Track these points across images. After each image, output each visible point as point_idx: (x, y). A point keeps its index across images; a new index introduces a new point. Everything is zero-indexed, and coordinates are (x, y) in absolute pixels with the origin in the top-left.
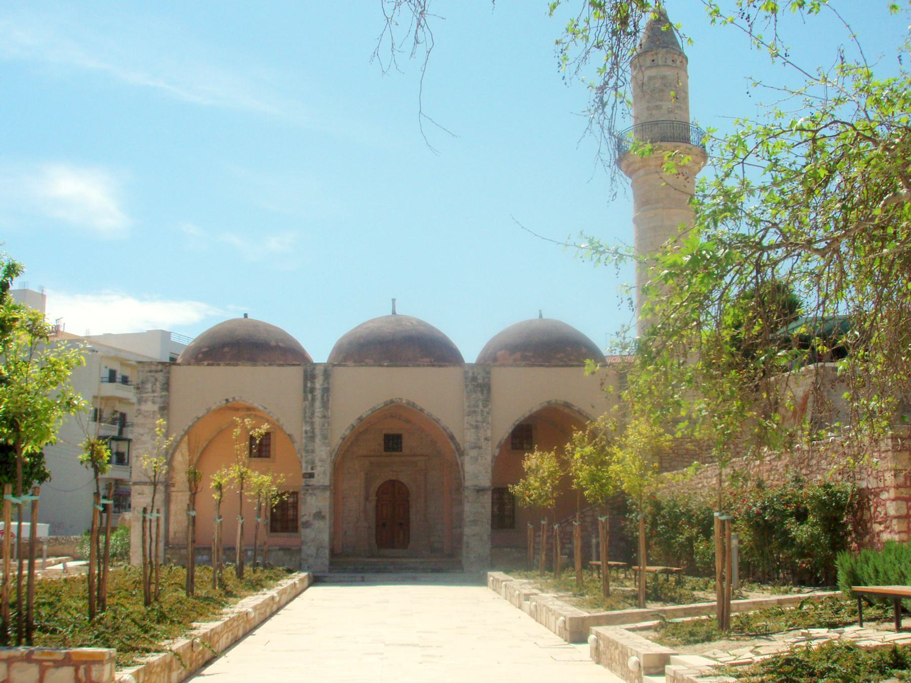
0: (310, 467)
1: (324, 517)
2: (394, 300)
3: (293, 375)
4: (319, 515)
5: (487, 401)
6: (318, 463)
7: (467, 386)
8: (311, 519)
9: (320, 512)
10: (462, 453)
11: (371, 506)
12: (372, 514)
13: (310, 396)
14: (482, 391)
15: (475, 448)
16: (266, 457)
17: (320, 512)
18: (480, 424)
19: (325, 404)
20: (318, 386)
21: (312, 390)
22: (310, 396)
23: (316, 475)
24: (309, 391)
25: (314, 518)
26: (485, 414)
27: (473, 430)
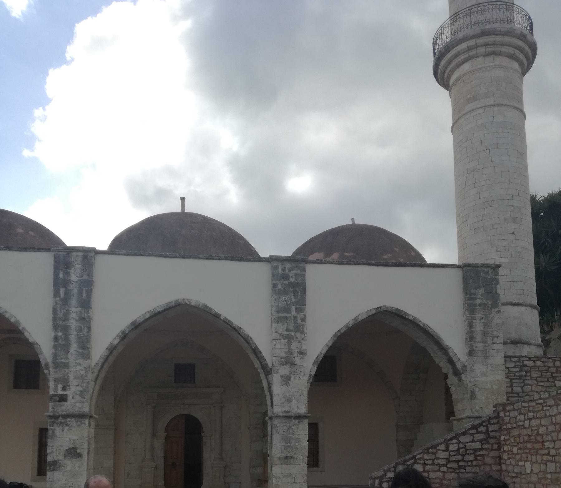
0: (60, 386)
1: (79, 455)
2: (183, 199)
3: (41, 263)
4: (73, 453)
5: (301, 304)
6: (73, 382)
7: (275, 286)
8: (60, 458)
9: (75, 449)
10: (268, 372)
11: (159, 444)
12: (160, 452)
13: (62, 291)
14: (295, 293)
15: (286, 363)
16: (34, 388)
17: (75, 449)
18: (293, 334)
19: (86, 304)
20: (74, 278)
21: (66, 283)
22: (62, 291)
23: (69, 398)
24: (60, 283)
25: (65, 456)
26: (299, 321)
27: (284, 342)
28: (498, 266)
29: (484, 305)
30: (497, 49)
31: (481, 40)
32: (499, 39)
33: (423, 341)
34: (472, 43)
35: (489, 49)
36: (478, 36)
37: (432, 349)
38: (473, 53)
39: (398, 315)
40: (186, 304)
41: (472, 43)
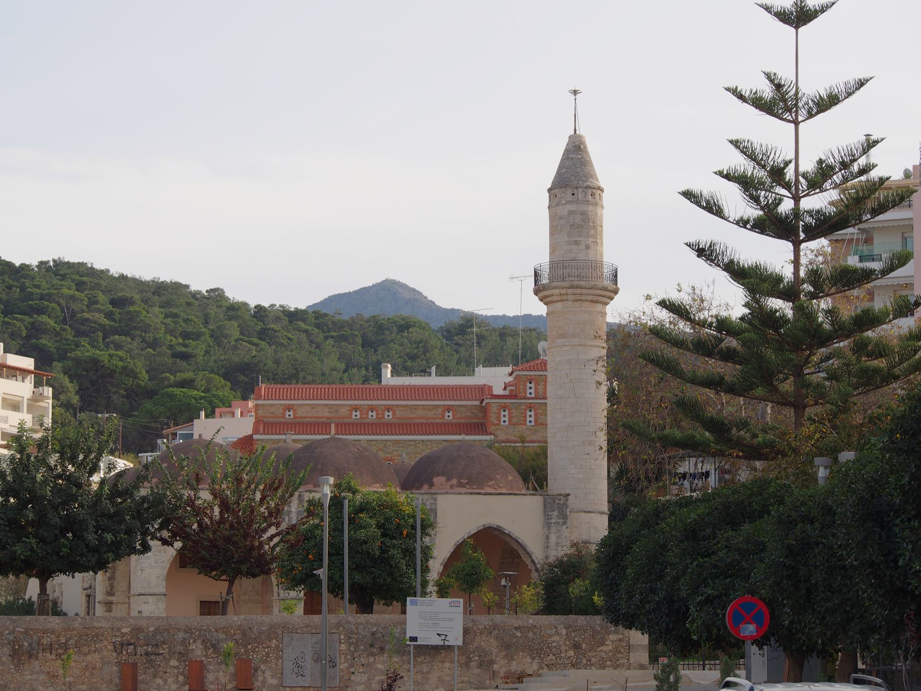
28: (568, 495)
29: (558, 523)
30: (584, 298)
31: (569, 291)
32: (584, 291)
33: (516, 547)
34: (563, 291)
35: (577, 297)
36: (569, 288)
37: (521, 552)
38: (565, 297)
39: (499, 530)
40: (387, 311)
41: (563, 291)
